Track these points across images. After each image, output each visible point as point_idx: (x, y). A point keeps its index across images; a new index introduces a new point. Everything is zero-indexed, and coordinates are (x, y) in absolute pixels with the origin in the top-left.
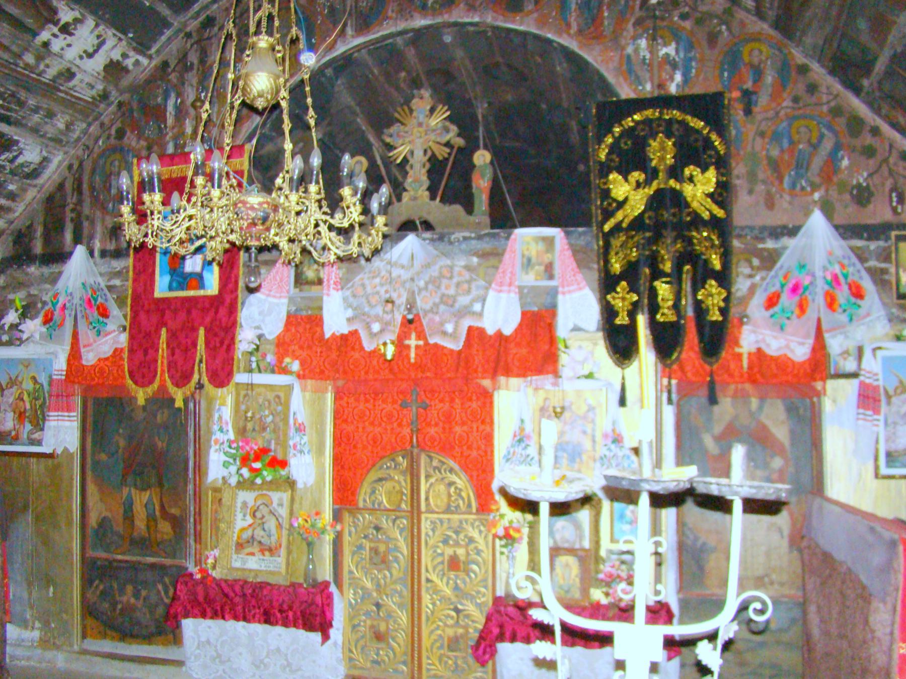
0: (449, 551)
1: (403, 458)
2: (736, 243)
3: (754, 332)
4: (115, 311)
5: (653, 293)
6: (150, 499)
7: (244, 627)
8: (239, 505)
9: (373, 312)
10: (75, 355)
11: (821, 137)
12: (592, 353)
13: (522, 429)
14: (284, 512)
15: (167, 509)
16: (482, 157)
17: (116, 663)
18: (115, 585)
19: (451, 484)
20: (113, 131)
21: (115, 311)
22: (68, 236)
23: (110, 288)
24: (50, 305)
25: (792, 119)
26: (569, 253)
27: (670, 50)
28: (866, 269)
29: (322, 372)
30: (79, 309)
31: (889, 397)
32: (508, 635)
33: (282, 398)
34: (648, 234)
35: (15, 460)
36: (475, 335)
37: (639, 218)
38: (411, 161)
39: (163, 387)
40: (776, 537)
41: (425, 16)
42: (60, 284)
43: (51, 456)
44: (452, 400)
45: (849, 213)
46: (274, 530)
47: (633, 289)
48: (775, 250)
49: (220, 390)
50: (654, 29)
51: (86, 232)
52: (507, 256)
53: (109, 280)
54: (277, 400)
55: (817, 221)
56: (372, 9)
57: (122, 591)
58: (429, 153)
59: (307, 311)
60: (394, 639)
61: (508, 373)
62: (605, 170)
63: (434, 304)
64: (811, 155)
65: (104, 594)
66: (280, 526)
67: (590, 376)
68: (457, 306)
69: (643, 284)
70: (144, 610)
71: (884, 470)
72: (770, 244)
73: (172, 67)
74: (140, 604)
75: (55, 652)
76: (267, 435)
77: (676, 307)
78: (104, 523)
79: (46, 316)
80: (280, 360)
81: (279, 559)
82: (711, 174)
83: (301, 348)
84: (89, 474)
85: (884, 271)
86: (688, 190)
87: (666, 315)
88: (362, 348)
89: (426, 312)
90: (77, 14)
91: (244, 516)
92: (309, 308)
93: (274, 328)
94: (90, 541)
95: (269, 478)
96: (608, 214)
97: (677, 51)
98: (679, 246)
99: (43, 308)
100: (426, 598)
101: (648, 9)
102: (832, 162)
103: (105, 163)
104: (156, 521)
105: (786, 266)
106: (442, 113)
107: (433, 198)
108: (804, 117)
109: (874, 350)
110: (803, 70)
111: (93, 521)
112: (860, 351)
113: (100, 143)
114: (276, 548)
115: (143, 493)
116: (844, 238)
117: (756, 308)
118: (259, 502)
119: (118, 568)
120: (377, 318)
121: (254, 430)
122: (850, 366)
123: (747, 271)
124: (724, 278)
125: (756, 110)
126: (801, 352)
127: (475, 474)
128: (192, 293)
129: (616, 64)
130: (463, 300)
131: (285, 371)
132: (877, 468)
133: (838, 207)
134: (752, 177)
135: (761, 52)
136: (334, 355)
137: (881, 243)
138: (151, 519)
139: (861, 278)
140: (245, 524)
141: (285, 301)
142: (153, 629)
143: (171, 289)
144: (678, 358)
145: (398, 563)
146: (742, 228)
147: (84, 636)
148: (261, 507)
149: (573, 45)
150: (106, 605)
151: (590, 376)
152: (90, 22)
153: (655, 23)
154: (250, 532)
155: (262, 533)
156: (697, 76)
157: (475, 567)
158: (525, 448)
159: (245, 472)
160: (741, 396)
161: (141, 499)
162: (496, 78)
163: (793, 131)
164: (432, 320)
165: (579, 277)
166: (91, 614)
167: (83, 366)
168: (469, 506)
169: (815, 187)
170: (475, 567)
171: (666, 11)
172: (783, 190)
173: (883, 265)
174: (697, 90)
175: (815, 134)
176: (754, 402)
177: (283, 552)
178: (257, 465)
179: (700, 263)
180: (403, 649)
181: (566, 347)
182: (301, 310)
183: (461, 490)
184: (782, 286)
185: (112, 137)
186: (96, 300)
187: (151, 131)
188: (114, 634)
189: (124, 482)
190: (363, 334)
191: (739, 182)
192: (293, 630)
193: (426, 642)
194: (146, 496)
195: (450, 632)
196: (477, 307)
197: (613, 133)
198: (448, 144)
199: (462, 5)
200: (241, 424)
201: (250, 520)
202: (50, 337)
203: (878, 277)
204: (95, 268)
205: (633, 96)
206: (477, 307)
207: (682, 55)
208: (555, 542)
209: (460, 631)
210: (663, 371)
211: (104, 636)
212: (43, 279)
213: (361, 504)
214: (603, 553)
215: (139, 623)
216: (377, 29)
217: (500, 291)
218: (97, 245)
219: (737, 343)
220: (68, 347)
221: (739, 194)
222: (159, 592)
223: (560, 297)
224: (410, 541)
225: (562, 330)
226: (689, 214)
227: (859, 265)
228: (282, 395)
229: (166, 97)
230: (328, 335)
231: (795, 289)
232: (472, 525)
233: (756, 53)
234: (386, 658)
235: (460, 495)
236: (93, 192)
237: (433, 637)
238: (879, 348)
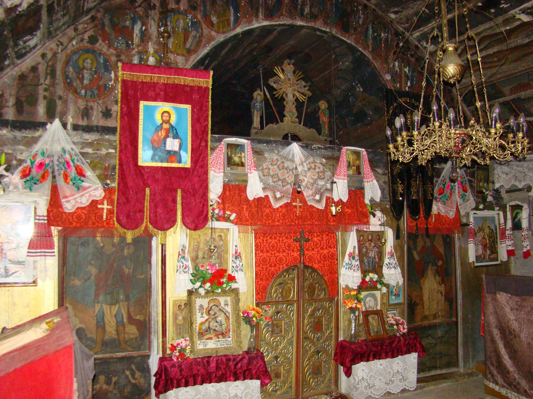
4: (89, 173)
6: (119, 311)
7: (213, 386)
8: (197, 307)
14: (229, 309)
15: (134, 317)
20: (86, 36)
21: (89, 173)
22: (41, 110)
38: (286, 99)
40: (440, 295)
42: (37, 148)
46: (224, 322)
51: (59, 108)
53: (82, 148)
54: (220, 238)
56: (274, 6)
59: (235, 182)
66: (227, 318)
73: (139, 3)
79: (24, 171)
81: (230, 339)
88: (271, 206)
91: (202, 314)
92: (237, 180)
103: (79, 58)
104: (124, 326)
107: (300, 123)
113: (74, 43)
114: (226, 332)
115: (113, 307)
118: (211, 305)
121: (204, 258)
126: (452, 215)
131: (226, 219)
138: (120, 324)
139: (466, 183)
140: (203, 320)
143: (153, 159)
148: (213, 308)
154: (207, 325)
155: (216, 324)
162: (59, 41)
182: (232, 181)
185: (85, 41)
187: (120, 43)
189: (96, 300)
194: (115, 309)
197: (393, 106)
201: (206, 317)
204: (68, 138)
216: (277, 19)
218: (70, 121)
222: (127, 377)
224: (20, 328)
228: (223, 234)
229: (134, 22)
230: (251, 198)
236: (66, 79)
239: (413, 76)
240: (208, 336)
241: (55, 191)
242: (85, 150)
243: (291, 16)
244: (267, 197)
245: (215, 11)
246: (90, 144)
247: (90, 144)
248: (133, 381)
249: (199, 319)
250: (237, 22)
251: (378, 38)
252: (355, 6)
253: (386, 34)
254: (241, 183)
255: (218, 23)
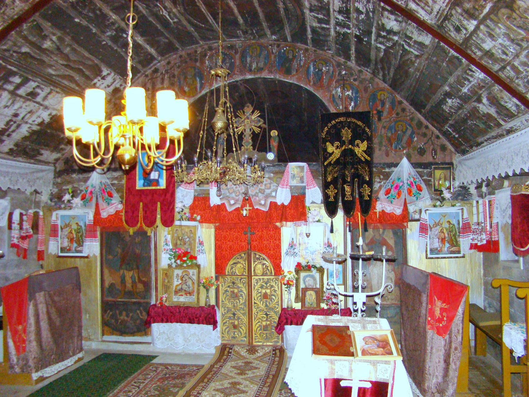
0: (264, 291)
1: (244, 254)
2: (374, 169)
3: (381, 204)
4: (115, 195)
5: (343, 189)
8: (175, 275)
9: (231, 196)
10: (97, 213)
11: (407, 129)
12: (319, 212)
13: (293, 242)
14: (195, 278)
16: (274, 133)
17: (120, 345)
18: (118, 312)
19: (264, 264)
21: (115, 195)
23: (112, 184)
24: (84, 191)
25: (396, 122)
26: (310, 173)
27: (350, 93)
28: (423, 180)
29: (210, 220)
30: (98, 193)
31: (431, 228)
32: (289, 321)
33: (193, 231)
34: (341, 167)
35: (69, 259)
36: (273, 205)
37: (338, 160)
38: (245, 134)
39: (141, 227)
41: (251, 75)
42: (89, 183)
43: (87, 257)
44: (262, 231)
45: (417, 158)
46: (191, 285)
47: (335, 188)
48: (389, 172)
49: (163, 227)
50: (344, 85)
52: (285, 174)
55: (405, 161)
57: (121, 314)
58: (252, 130)
60: (241, 327)
61: (287, 220)
62: (325, 141)
63: (256, 193)
64: (403, 136)
65: (112, 317)
66: (193, 283)
67: (319, 221)
68: (265, 193)
69: (339, 186)
70: (131, 322)
71: (429, 256)
72: (387, 170)
74: (129, 319)
75: (90, 342)
76: (187, 246)
77: (352, 195)
78: (112, 285)
80: (192, 216)
81: (194, 297)
82: (365, 143)
83: (201, 210)
84: (104, 264)
85: (430, 181)
86: (356, 150)
87: (348, 198)
88: (226, 210)
89: (253, 196)
90: (109, 72)
92: (203, 194)
93: (188, 201)
94: (106, 292)
95: (190, 264)
96: (326, 159)
97: (352, 93)
98: (353, 171)
99: (81, 193)
100: (254, 310)
101: (341, 76)
102: (411, 138)
105: (393, 178)
106: (257, 114)
107: (254, 149)
108: (400, 121)
109: (426, 210)
110: (400, 103)
111: (107, 285)
112: (420, 211)
116: (414, 168)
117: (382, 194)
118: (184, 274)
119: (118, 304)
120: (233, 199)
121: (181, 244)
122: (417, 216)
123: (378, 180)
124: (370, 184)
125: (382, 118)
126: (398, 211)
127: (272, 260)
128: (154, 188)
129: (328, 98)
130: (268, 191)
132: (427, 255)
133: (413, 156)
134: (380, 143)
135: (384, 95)
136: (215, 213)
137: (429, 170)
138: (134, 283)
140: (178, 283)
141: (193, 191)
142: (136, 330)
143: (144, 186)
144: (353, 214)
145: (242, 297)
146: (377, 164)
147: (103, 335)
149: (311, 89)
150: (113, 321)
151: (319, 221)
152: (113, 74)
153: (344, 82)
154: (180, 286)
155: (186, 286)
156: (360, 103)
157: (274, 297)
158: (294, 249)
159: (179, 262)
160: (376, 228)
161: (129, 275)
163: (396, 126)
164: (255, 199)
165: (314, 182)
166: (107, 325)
167: (101, 218)
168: (271, 273)
169: (404, 148)
170: (274, 297)
171: (349, 77)
172: (392, 149)
173: (429, 178)
174: (360, 110)
175: (404, 128)
176: (381, 231)
177: (195, 294)
178: (185, 259)
179: (361, 178)
180: (245, 331)
181: (310, 210)
183: (268, 267)
184: (392, 186)
186: (106, 189)
188: (117, 333)
190: (227, 205)
191: (376, 146)
192: (201, 325)
193: (254, 328)
194: (131, 273)
195: (264, 323)
196: (274, 194)
198: (260, 127)
199: (266, 71)
200: (175, 242)
201: (180, 282)
202: (85, 205)
203: (428, 183)
205: (335, 111)
206: (274, 194)
207: (354, 95)
208: (306, 286)
209: (268, 323)
210: (347, 219)
211: (112, 334)
212: (79, 180)
213: (227, 273)
214: (325, 289)
215: (128, 328)
217: (283, 188)
219: (375, 209)
220: (94, 210)
221: (376, 151)
222: (138, 314)
223: (307, 190)
225: (308, 204)
226: (357, 159)
227: (420, 179)
230: (212, 205)
231: (396, 187)
232: (272, 280)
233: (383, 95)
234: (237, 336)
235: (267, 269)
237: (257, 326)
238: (427, 210)
239: (356, 97)
240: (180, 294)
241: (97, 205)
242: (114, 182)
243: (242, 73)
244: (223, 204)
245: (187, 84)
246: (116, 178)
247: (116, 178)
248: (141, 317)
249: (176, 282)
250: (202, 88)
251: (320, 73)
252: (297, 53)
253: (327, 68)
254: (206, 195)
255: (189, 90)
